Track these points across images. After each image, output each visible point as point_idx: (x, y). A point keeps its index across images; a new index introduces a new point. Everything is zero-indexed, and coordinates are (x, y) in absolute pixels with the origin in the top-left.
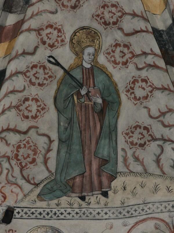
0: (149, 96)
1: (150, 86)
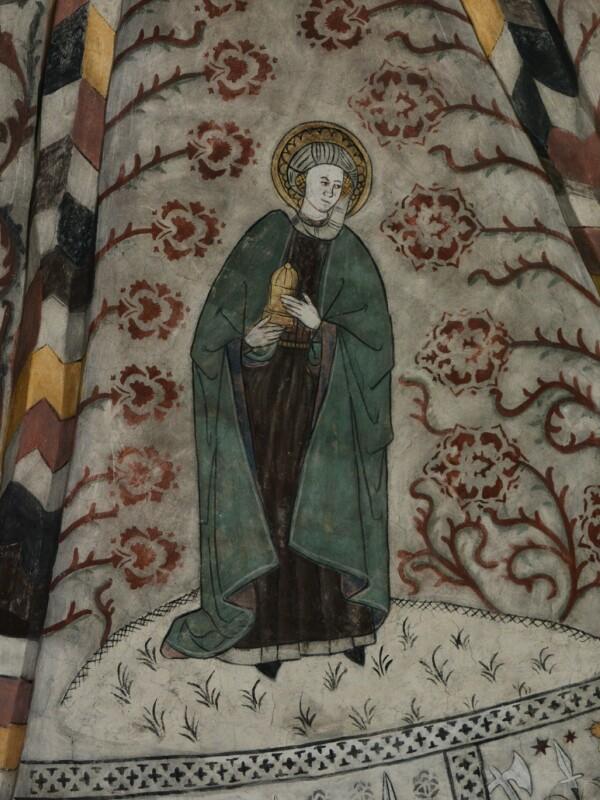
0: (497, 368)
1: (464, 219)
